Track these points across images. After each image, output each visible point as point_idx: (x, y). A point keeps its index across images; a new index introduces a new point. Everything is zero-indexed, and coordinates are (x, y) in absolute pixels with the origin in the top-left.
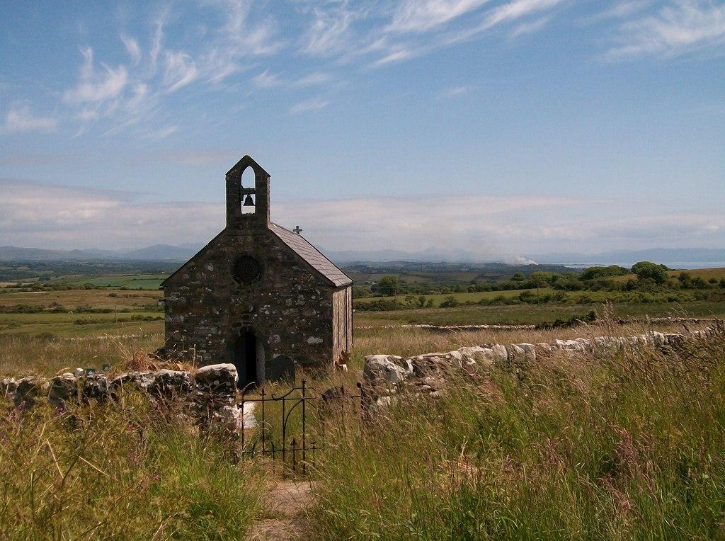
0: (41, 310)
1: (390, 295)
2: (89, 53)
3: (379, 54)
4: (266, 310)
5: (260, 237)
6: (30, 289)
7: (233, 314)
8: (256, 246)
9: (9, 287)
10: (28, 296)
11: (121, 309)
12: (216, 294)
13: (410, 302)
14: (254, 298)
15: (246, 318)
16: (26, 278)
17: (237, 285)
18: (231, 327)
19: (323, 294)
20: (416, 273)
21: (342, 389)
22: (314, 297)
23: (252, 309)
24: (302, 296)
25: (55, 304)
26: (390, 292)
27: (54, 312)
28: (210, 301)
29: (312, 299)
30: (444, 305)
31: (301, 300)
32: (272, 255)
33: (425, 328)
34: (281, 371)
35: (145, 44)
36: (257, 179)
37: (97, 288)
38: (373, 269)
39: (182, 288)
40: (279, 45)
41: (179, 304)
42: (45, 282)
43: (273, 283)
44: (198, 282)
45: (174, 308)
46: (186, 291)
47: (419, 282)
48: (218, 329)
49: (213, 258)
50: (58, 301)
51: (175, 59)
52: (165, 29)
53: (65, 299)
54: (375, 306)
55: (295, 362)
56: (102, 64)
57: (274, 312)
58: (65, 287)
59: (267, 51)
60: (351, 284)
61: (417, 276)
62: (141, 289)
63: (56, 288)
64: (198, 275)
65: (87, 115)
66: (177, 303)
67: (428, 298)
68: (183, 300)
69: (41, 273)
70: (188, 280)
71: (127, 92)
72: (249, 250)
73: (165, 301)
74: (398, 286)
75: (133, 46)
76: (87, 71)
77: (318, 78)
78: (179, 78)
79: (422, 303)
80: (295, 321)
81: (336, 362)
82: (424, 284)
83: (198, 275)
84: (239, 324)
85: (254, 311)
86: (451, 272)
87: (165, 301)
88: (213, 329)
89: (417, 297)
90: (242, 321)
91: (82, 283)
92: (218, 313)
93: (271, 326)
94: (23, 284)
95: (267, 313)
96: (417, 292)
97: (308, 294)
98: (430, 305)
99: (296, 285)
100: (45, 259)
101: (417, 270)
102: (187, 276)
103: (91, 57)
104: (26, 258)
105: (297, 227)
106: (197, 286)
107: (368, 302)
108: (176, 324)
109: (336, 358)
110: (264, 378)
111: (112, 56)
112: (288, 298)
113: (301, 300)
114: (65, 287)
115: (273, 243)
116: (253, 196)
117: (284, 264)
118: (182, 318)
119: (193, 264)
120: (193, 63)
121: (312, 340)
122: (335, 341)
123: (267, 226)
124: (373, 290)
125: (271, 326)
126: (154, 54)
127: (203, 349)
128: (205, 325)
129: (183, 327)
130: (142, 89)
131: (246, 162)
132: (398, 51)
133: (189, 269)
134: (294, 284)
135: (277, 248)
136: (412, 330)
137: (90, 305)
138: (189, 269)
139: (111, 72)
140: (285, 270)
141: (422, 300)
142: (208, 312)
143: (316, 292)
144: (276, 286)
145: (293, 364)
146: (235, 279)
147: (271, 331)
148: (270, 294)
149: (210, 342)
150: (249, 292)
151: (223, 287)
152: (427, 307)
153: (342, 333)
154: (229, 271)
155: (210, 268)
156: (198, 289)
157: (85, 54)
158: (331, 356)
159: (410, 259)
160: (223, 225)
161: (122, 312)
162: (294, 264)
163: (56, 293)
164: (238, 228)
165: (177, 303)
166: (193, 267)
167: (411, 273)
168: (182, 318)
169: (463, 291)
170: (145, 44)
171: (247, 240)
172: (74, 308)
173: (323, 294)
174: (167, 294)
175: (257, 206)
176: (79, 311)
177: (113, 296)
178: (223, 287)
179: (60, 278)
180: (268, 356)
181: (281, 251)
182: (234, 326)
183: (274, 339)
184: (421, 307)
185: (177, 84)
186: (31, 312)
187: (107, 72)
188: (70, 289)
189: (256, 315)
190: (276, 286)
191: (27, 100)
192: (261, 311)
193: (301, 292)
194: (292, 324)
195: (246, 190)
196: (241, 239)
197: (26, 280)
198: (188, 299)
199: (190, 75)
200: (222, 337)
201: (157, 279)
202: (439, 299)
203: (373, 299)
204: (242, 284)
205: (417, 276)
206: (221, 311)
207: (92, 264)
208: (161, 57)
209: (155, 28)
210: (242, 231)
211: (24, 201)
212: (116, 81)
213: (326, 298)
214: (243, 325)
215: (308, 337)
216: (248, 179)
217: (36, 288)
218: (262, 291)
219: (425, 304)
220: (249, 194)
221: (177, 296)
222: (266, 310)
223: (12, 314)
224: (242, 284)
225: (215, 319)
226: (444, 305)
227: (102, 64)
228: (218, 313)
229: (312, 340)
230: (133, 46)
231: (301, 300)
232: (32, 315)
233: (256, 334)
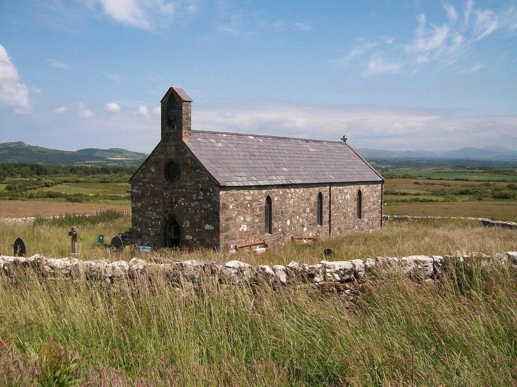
2: (422, 18)
11: (414, 193)
12: (156, 189)
28: (154, 194)
35: (460, 9)
43: (186, 181)
48: (157, 214)
49: (155, 162)
51: (483, 16)
56: (431, 24)
60: (382, 182)
62: (441, 179)
65: (421, 60)
69: (383, 167)
71: (448, 42)
73: (131, 192)
75: (452, 12)
76: (420, 31)
78: (485, 30)
87: (131, 192)
90: (169, 209)
97: (205, 191)
105: (344, 136)
111: (437, 18)
112: (194, 193)
114: (389, 177)
117: (192, 168)
120: (497, 17)
121: (208, 227)
123: (180, 139)
126: (467, 15)
127: (150, 227)
128: (151, 211)
130: (459, 39)
133: (142, 170)
139: (438, 30)
144: (187, 184)
146: (166, 178)
161: (415, 195)
162: (198, 168)
166: (145, 169)
168: (140, 204)
170: (460, 9)
177: (417, 183)
179: (396, 170)
185: (482, 35)
187: (435, 29)
188: (392, 178)
189: (177, 205)
190: (187, 184)
192: (179, 202)
193: (202, 189)
194: (196, 214)
196: (168, 149)
198: (143, 191)
199: (493, 26)
200: (159, 219)
201: (456, 172)
207: (418, 161)
208: (473, 17)
211: (416, 122)
212: (440, 35)
214: (170, 212)
215: (205, 224)
218: (180, 187)
221: (138, 190)
225: (156, 206)
227: (431, 24)
228: (157, 202)
230: (452, 12)
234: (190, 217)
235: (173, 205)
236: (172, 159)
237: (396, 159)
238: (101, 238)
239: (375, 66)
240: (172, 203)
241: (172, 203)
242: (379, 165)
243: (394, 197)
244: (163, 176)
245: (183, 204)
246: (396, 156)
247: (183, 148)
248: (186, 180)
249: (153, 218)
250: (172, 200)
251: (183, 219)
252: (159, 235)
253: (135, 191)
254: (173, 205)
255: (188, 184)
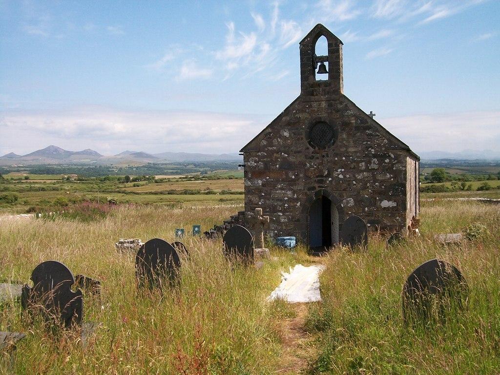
0: (199, 193)
1: (439, 182)
2: (232, 26)
3: (427, 14)
4: (339, 174)
5: (333, 102)
6: (192, 179)
7: (307, 177)
8: (330, 111)
9: (180, 178)
10: (192, 184)
12: (292, 159)
13: (455, 187)
14: (328, 162)
15: (321, 182)
16: (192, 172)
17: (312, 149)
18: (306, 191)
19: (397, 157)
20: (456, 167)
21: (58, 199)
22: (387, 161)
23: (326, 173)
24: (376, 160)
25: (208, 189)
26: (440, 180)
27: (207, 194)
28: (287, 166)
29: (386, 163)
30: (481, 189)
31: (375, 164)
32: (346, 119)
33: (481, 201)
34: (355, 237)
35: (267, 18)
36: (330, 45)
37: (236, 178)
38: (426, 165)
39: (260, 154)
40: (357, 12)
41: (257, 169)
42: (204, 175)
43: (347, 147)
44: (275, 148)
45: (253, 173)
46: (264, 157)
47: (459, 174)
49: (289, 124)
50: (211, 187)
52: (280, 7)
53: (215, 186)
54: (428, 189)
55: (369, 225)
56: (240, 33)
57: (348, 176)
58: (216, 178)
59: (349, 17)
61: (458, 169)
63: (210, 178)
64: (275, 142)
65: (231, 66)
66: (255, 168)
67: (468, 184)
68: (261, 165)
69: (201, 170)
70: (265, 146)
71: (257, 50)
72: (324, 115)
73: (244, 166)
74: (445, 175)
75: (259, 20)
76: (230, 38)
77: (384, 33)
79: (464, 187)
80: (368, 185)
81: (409, 226)
82: (463, 175)
83: (275, 142)
84: (314, 188)
85: (329, 175)
86: (483, 166)
87: (244, 166)
88: (289, 193)
89: (460, 183)
90: (316, 185)
91: (226, 175)
92: (293, 177)
93: (344, 190)
94: (189, 176)
95: (341, 176)
96: (459, 180)
97: (381, 157)
98: (469, 189)
99: (370, 149)
100: (204, 160)
101: (458, 165)
102: (264, 142)
103: (233, 29)
104: (192, 159)
105: (371, 112)
106: (273, 152)
107: (424, 187)
108: (254, 188)
109: (409, 222)
110: (337, 239)
111: (246, 26)
112: (362, 161)
113: (374, 163)
114: (216, 178)
115: (346, 108)
116: (326, 64)
117: (357, 128)
118: (260, 182)
119: (270, 130)
121: (385, 204)
122: (408, 207)
124: (426, 179)
125: (344, 190)
126: (273, 24)
127: (280, 211)
128: (282, 189)
129: (261, 192)
130: (266, 47)
131: (319, 31)
132: (441, 11)
134: (367, 148)
135: (350, 112)
136: (468, 202)
137: (231, 189)
138: (266, 135)
140: (359, 134)
141: (463, 185)
142: (284, 177)
143: (390, 156)
145: (365, 226)
146: (310, 144)
147: (344, 194)
148: (344, 158)
149: (286, 205)
150: (323, 156)
151: (299, 152)
152: (467, 190)
153: (413, 201)
154: (303, 136)
155: (286, 134)
156: (275, 155)
157: (229, 27)
158: (404, 220)
159: (452, 157)
160: (297, 92)
162: (369, 128)
163: (209, 182)
164: (313, 95)
165: (255, 168)
166: (270, 133)
167: (453, 167)
168: (260, 182)
169: (494, 179)
170: (267, 18)
171: (321, 106)
172: (220, 191)
173: (397, 157)
174: (246, 159)
175: (330, 73)
176: (223, 193)
178: (299, 152)
180: (341, 219)
181: (354, 116)
182: (309, 189)
183: (348, 202)
184: (463, 190)
186: (193, 194)
188: (218, 179)
189: (330, 179)
191: (193, 58)
192: (335, 174)
193: (375, 156)
194: (365, 188)
195: (320, 58)
196: (315, 104)
197: (192, 174)
198: (265, 164)
200: (297, 200)
202: (476, 185)
203: (427, 185)
204: (317, 148)
205: (458, 169)
206: (297, 175)
208: (278, 26)
209: (273, 7)
210: (316, 97)
212: (249, 43)
213: (399, 162)
214: (318, 189)
215: (381, 201)
216: (322, 48)
217: (196, 178)
218: (336, 155)
219: (466, 188)
220: (322, 62)
222: (339, 174)
223: (180, 196)
224: (317, 148)
225: (291, 183)
226: (481, 189)
227: (240, 33)
228: (293, 177)
229: (385, 204)
230: (259, 20)
231: (374, 163)
232: (194, 195)
233: (330, 198)
234: (355, 193)
235: (324, 179)
236: (320, 118)
237: (213, 162)
238: (196, 229)
239: (188, 71)
240: (322, 176)
241: (322, 176)
242: (198, 168)
243: (233, 196)
244: (305, 141)
245: (341, 176)
246: (212, 159)
247: (341, 103)
248: (349, 145)
249: (286, 198)
250: (321, 171)
251: (341, 196)
252: (298, 220)
253: (252, 163)
254: (324, 179)
255: (352, 150)
